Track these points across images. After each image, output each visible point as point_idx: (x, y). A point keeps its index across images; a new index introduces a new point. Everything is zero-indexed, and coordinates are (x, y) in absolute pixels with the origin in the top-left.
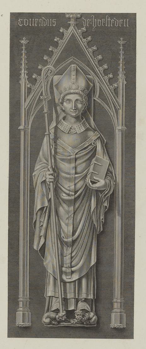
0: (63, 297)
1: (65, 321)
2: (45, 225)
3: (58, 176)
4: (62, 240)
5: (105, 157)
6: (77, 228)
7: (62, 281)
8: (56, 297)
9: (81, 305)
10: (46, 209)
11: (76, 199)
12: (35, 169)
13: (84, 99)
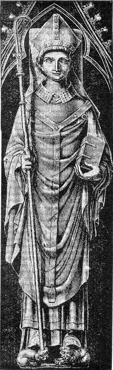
0: (44, 328)
1: (47, 361)
2: (20, 230)
3: (37, 162)
4: (43, 249)
5: (99, 134)
6: (63, 233)
7: (43, 305)
8: (35, 329)
9: (70, 340)
10: (21, 208)
11: (62, 194)
12: (6, 153)
13: (70, 58)
